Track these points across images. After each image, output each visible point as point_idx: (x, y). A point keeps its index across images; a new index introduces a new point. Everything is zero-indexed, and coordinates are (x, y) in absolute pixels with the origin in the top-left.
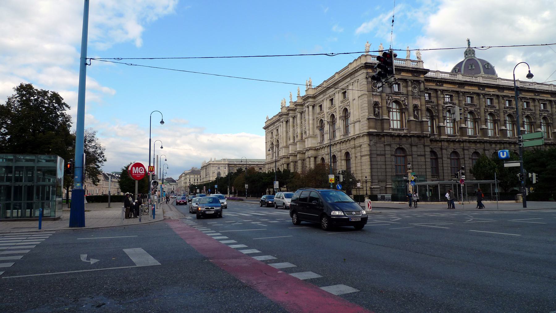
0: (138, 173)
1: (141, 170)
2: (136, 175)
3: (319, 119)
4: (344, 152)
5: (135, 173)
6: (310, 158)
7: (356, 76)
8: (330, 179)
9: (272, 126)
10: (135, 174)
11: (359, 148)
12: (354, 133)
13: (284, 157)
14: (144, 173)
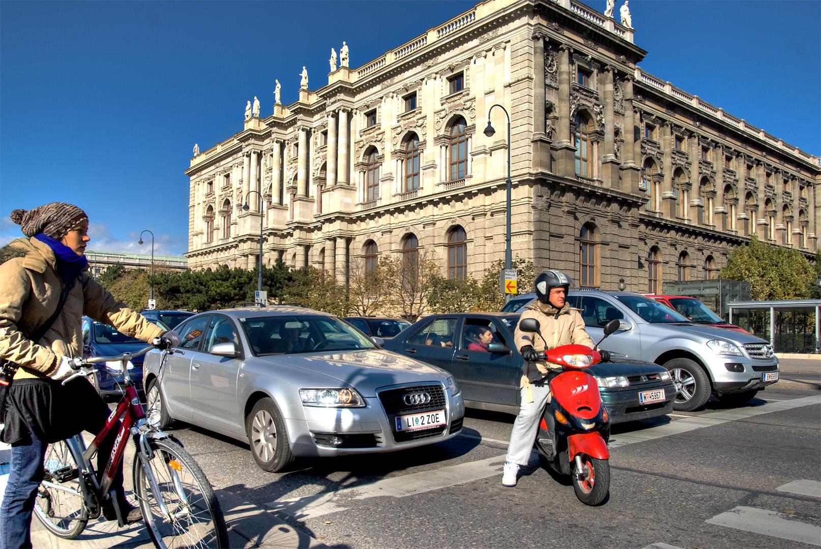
3: (364, 145)
4: (400, 233)
6: (334, 240)
7: (395, 82)
8: (507, 281)
9: (213, 167)
12: (485, 178)
13: (250, 238)
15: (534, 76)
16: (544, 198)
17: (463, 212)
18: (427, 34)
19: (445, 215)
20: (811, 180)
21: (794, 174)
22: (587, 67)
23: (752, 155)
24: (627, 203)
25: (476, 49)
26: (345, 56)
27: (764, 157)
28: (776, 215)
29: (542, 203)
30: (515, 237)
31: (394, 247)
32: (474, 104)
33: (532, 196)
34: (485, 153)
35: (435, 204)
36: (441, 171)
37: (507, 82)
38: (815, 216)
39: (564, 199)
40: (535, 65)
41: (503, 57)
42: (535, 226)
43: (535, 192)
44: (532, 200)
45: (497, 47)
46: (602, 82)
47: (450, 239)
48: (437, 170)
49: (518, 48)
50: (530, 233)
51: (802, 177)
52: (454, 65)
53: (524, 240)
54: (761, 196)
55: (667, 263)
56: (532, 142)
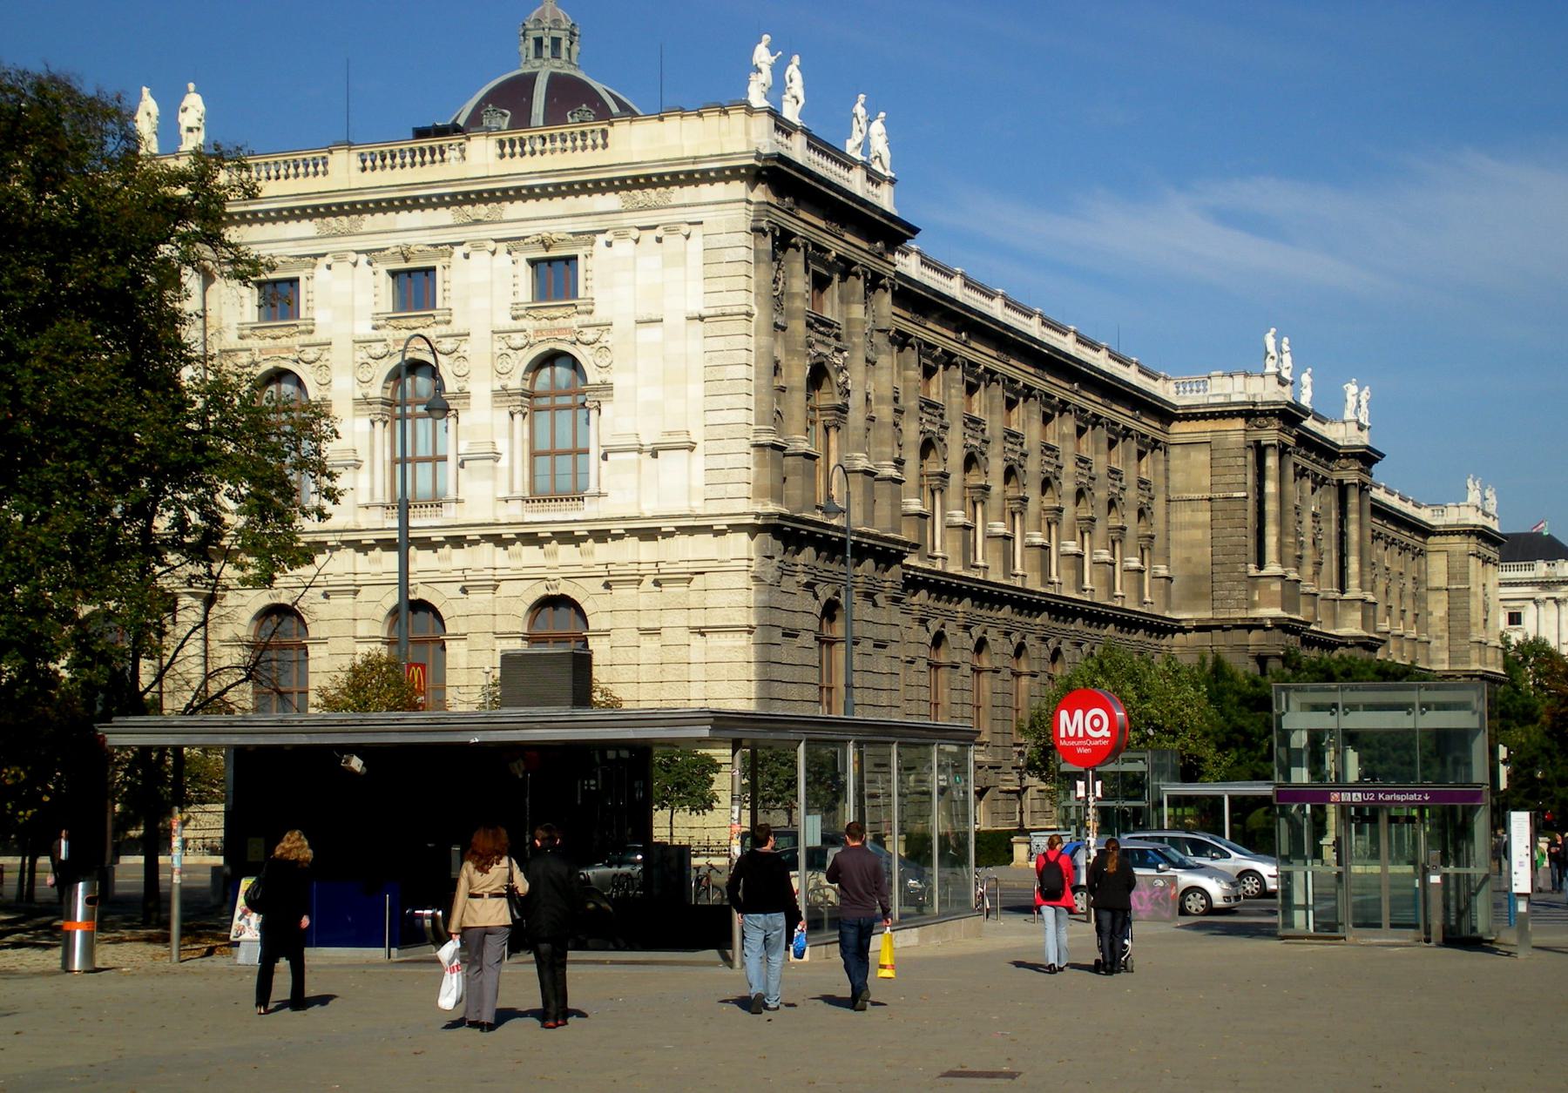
0: (1081, 734)
1: (1097, 723)
2: (1073, 743)
5: (1072, 734)
10: (1081, 739)
11: (351, 601)
14: (1108, 734)
15: (755, 310)
16: (775, 562)
17: (580, 569)
18: (468, 139)
19: (525, 571)
20: (1159, 436)
21: (1130, 425)
22: (825, 272)
23: (1054, 393)
24: (886, 555)
25: (615, 216)
26: (195, 124)
27: (1076, 393)
28: (1093, 527)
29: (771, 572)
30: (715, 635)
31: (363, 629)
32: (605, 337)
33: (753, 556)
34: (640, 451)
35: (498, 541)
36: (512, 468)
37: (698, 308)
38: (1168, 522)
39: (800, 558)
40: (758, 287)
41: (685, 254)
42: (759, 616)
43: (759, 549)
44: (753, 563)
45: (671, 229)
46: (845, 300)
47: (532, 623)
48: (504, 462)
49: (722, 245)
50: (750, 630)
51: (1143, 429)
52: (554, 237)
53: (737, 644)
54: (1069, 486)
55: (912, 662)
56: (754, 446)
